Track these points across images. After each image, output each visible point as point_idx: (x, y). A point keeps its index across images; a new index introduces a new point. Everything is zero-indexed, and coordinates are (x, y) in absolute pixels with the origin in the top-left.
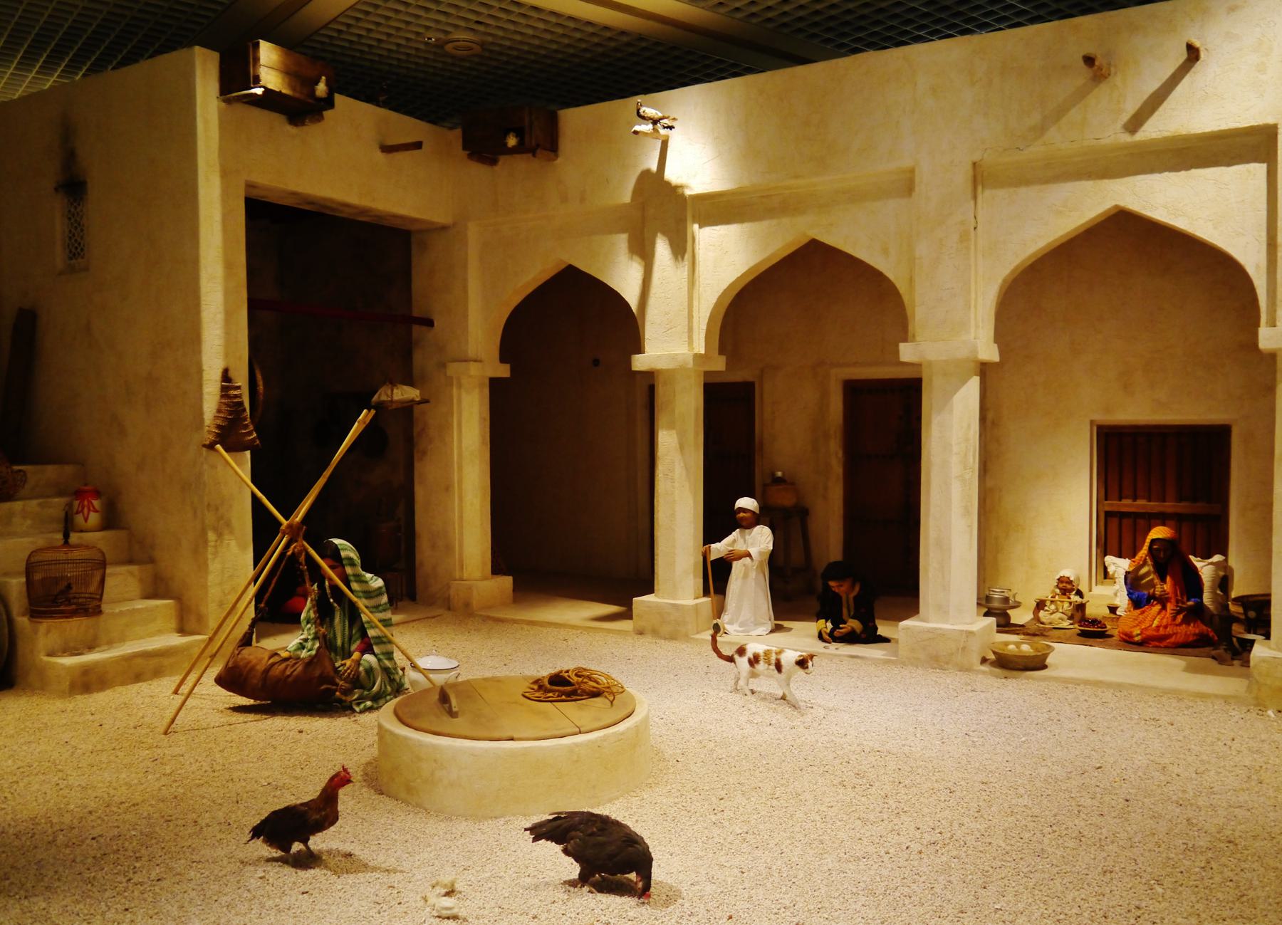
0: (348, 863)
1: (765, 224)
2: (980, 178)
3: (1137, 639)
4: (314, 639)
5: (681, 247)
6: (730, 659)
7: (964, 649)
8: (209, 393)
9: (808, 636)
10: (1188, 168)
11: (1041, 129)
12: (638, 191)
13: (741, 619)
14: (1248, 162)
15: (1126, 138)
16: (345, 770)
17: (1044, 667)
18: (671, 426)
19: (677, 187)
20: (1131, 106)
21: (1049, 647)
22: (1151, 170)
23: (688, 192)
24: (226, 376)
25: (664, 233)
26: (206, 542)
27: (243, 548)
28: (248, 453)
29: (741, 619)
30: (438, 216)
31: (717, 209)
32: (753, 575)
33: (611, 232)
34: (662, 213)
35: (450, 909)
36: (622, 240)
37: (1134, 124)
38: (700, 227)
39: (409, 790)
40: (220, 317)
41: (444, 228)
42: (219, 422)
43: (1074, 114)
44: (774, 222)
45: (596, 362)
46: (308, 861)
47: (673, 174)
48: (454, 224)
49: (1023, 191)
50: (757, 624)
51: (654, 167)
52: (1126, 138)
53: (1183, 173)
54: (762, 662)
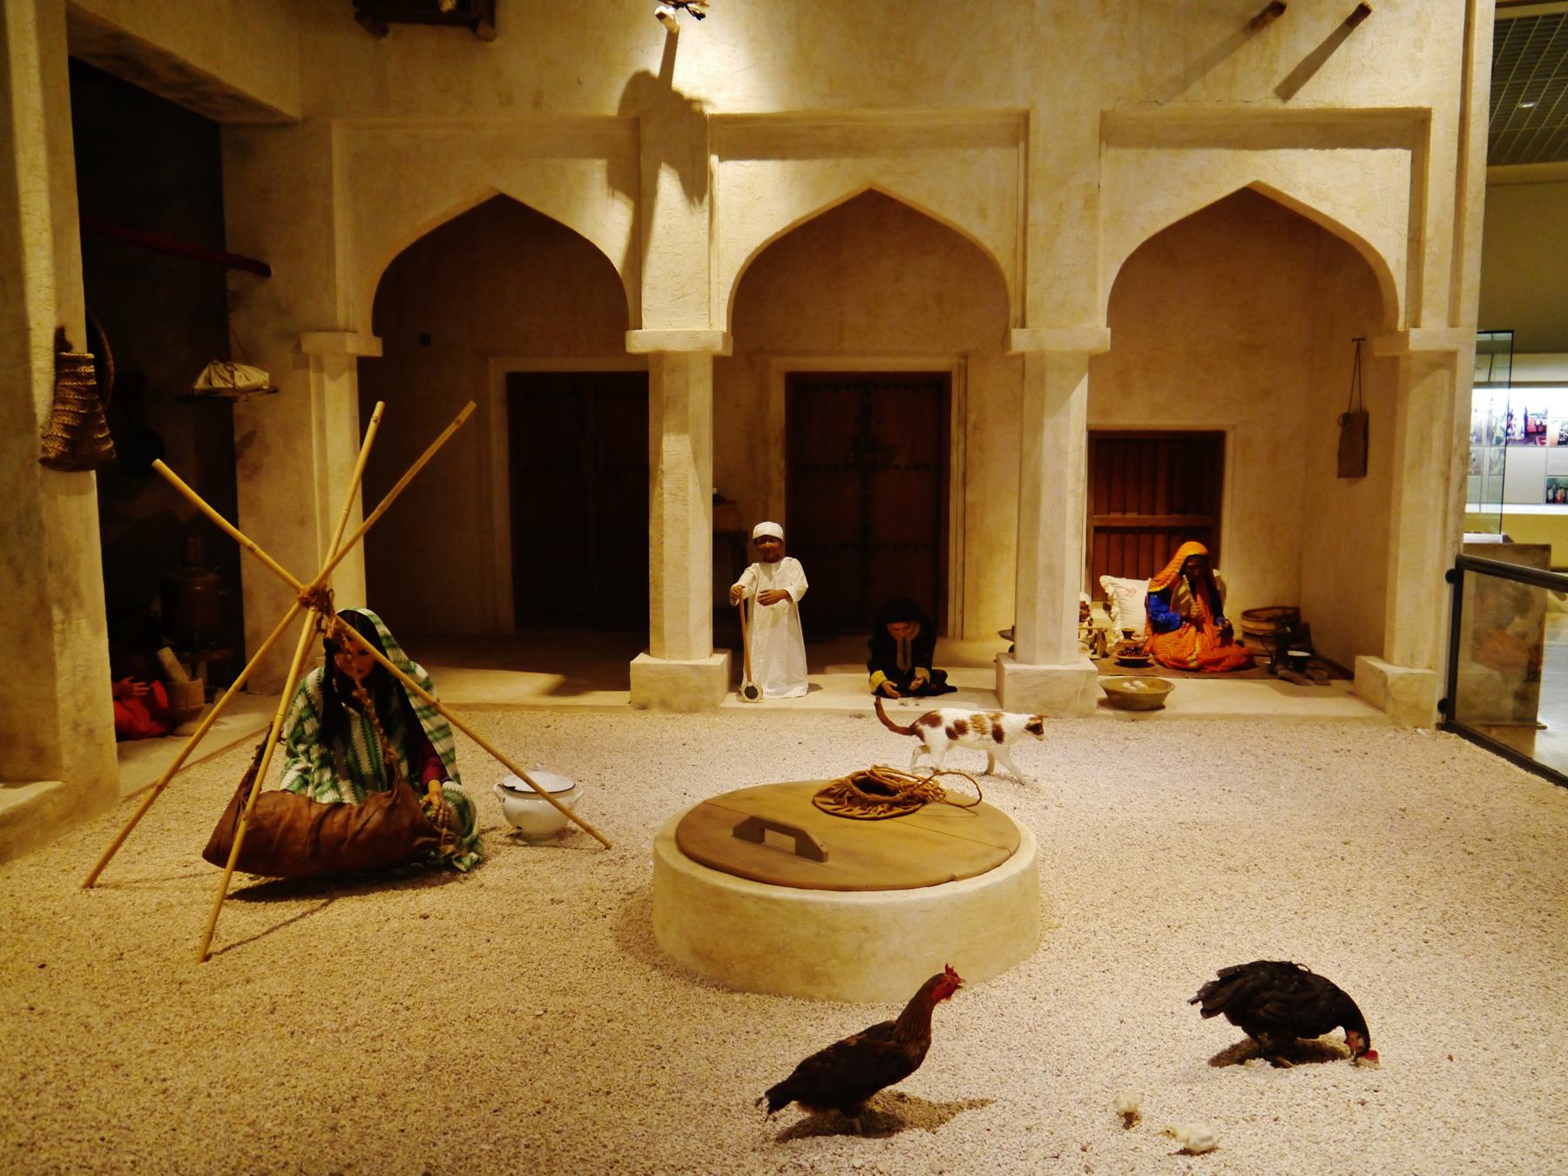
0: (936, 1116)
1: (817, 164)
2: (1111, 133)
3: (1193, 665)
4: (320, 767)
5: (697, 187)
6: (912, 731)
7: (1084, 692)
8: (40, 371)
9: (862, 691)
10: (1334, 147)
11: (1183, 83)
12: (628, 100)
13: (770, 678)
14: (1394, 147)
15: (1277, 104)
16: (949, 970)
17: (1162, 707)
18: (682, 429)
19: (691, 102)
20: (1285, 68)
21: (1168, 684)
22: (1295, 145)
23: (709, 111)
24: (60, 334)
25: (671, 164)
26: (49, 624)
27: (96, 631)
28: (93, 473)
29: (770, 678)
30: (289, 107)
31: (751, 138)
32: (785, 620)
33: (587, 156)
34: (663, 136)
35: (1210, 1138)
36: (597, 169)
37: (1288, 89)
38: (721, 160)
39: (811, 976)
40: (47, 237)
41: (286, 124)
42: (67, 420)
43: (1221, 69)
44: (830, 163)
45: (425, 340)
46: (886, 1126)
47: (685, 80)
48: (305, 120)
49: (1153, 153)
50: (791, 682)
51: (655, 68)
52: (1277, 104)
53: (1328, 151)
54: (971, 732)
